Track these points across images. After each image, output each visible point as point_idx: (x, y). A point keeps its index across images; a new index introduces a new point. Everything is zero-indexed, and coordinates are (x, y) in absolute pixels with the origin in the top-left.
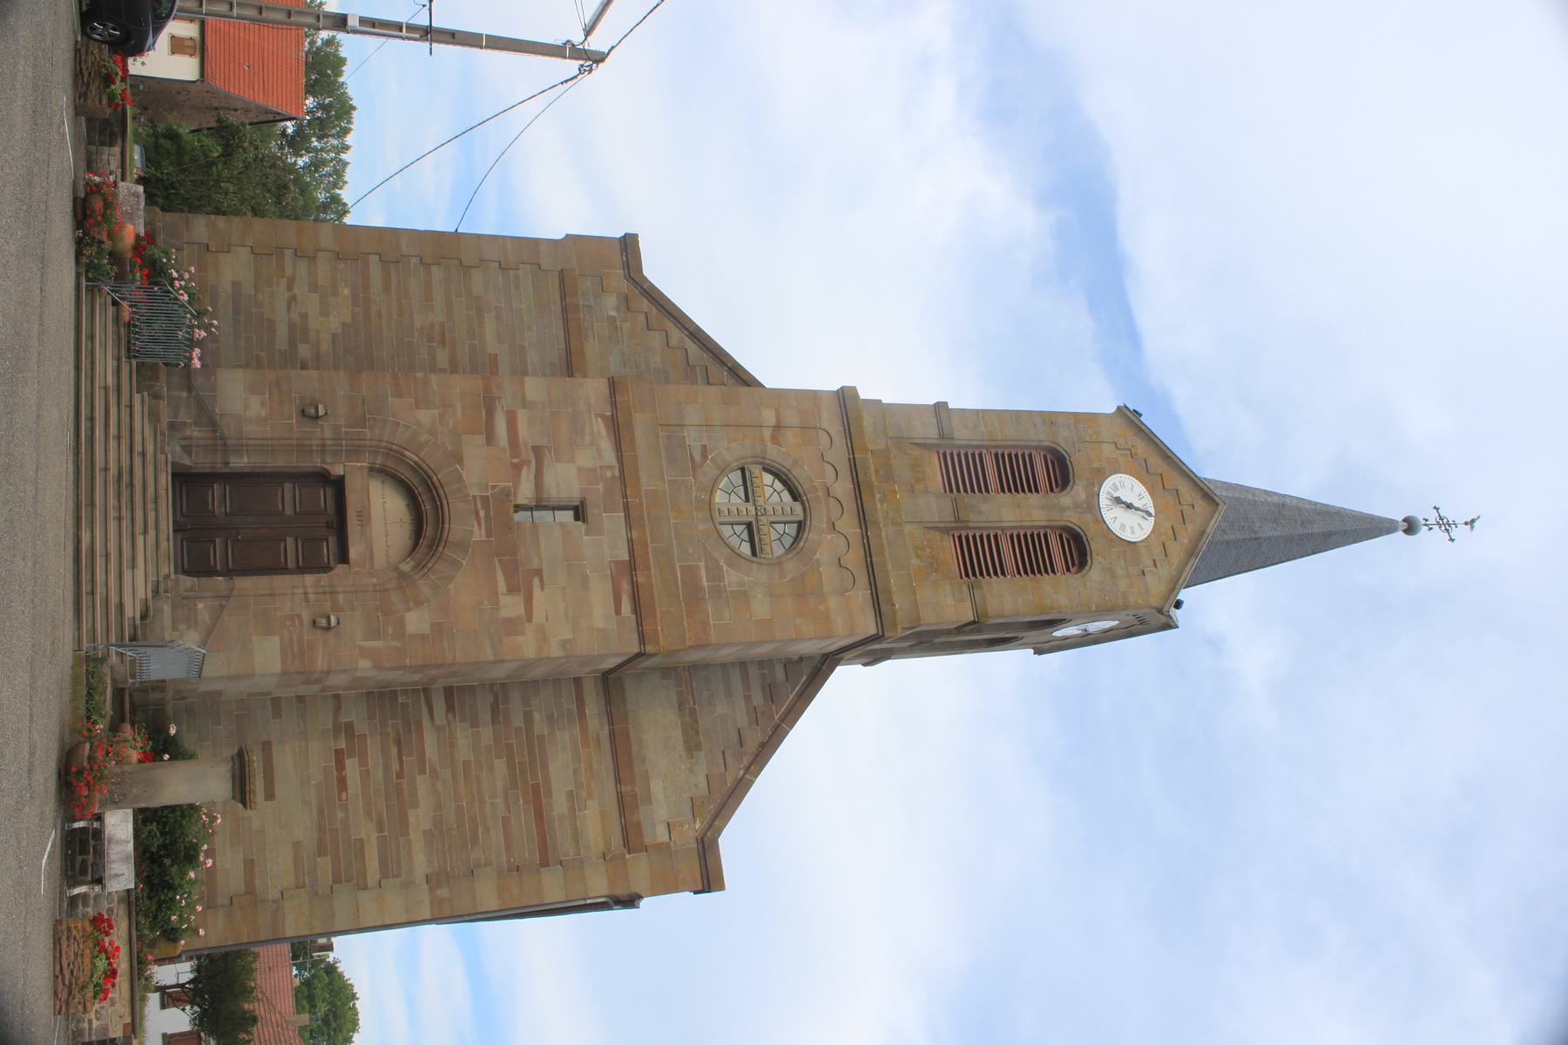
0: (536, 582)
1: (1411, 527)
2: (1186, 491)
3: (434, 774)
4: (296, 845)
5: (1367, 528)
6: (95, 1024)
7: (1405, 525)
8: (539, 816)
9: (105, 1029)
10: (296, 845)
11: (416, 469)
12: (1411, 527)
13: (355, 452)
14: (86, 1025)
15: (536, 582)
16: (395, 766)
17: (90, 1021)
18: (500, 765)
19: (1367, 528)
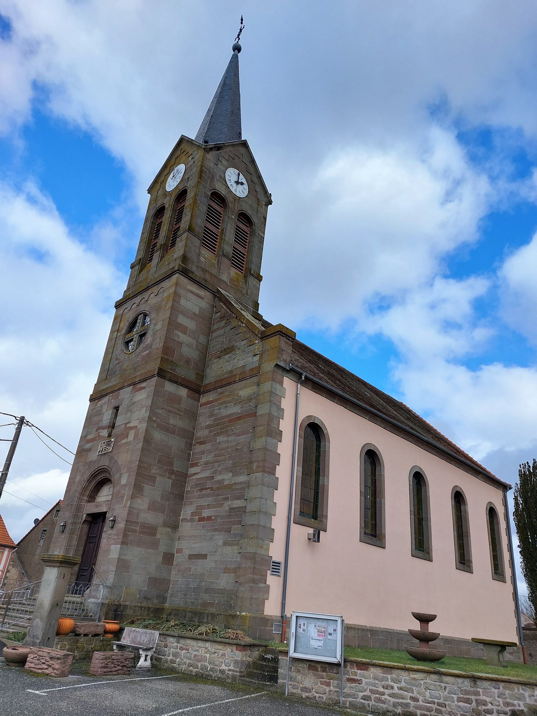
0: (128, 426)
1: (237, 48)
2: (178, 153)
3: (215, 472)
4: (225, 544)
5: (233, 67)
6: (232, 667)
7: (236, 51)
8: (239, 418)
9: (236, 662)
10: (225, 544)
11: (89, 481)
12: (237, 48)
13: (79, 509)
14: (231, 673)
15: (128, 426)
16: (209, 491)
17: (229, 670)
18: (219, 439)
19: (233, 67)
